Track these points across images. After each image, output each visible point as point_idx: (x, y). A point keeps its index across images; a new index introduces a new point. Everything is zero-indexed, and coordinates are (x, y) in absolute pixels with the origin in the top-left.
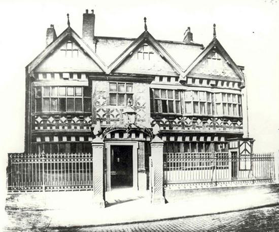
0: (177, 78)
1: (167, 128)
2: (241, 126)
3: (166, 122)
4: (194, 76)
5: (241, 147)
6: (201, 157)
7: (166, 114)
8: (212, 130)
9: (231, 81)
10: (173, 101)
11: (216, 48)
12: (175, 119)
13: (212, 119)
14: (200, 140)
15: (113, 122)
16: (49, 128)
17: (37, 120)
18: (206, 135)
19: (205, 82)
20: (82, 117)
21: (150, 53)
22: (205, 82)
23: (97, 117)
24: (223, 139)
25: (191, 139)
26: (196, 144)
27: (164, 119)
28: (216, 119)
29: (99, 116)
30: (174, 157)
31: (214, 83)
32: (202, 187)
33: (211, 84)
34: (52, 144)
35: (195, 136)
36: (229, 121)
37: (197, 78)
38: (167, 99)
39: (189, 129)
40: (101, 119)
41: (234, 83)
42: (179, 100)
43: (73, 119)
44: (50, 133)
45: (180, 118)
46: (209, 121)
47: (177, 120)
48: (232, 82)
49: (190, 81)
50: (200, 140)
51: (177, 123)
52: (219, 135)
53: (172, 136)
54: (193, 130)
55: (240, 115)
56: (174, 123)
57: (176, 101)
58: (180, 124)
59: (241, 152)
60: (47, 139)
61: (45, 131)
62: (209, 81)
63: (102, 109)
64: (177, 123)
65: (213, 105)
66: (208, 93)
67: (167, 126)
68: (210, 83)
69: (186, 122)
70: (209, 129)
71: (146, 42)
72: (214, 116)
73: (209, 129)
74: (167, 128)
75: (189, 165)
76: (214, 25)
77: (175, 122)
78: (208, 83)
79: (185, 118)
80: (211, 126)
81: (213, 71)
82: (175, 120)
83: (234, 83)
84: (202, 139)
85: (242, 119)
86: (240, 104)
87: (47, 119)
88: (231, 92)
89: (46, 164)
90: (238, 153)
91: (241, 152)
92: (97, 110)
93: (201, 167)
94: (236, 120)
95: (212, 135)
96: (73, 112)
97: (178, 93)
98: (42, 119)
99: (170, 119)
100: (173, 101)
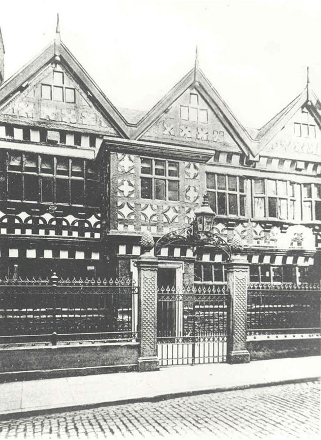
1: (74, 232)
10: (215, 189)
15: (145, 227)
16: (18, 232)
17: (97, 220)
19: (287, 164)
25: (261, 260)
37: (275, 158)
38: (227, 192)
39: (258, 243)
40: (127, 221)
41: (230, 156)
53: (207, 253)
54: (266, 245)
74: (74, 232)
76: (58, 15)
77: (89, 223)
82: (19, 215)
83: (230, 156)
84: (48, 254)
92: (119, 204)
98: (4, 215)
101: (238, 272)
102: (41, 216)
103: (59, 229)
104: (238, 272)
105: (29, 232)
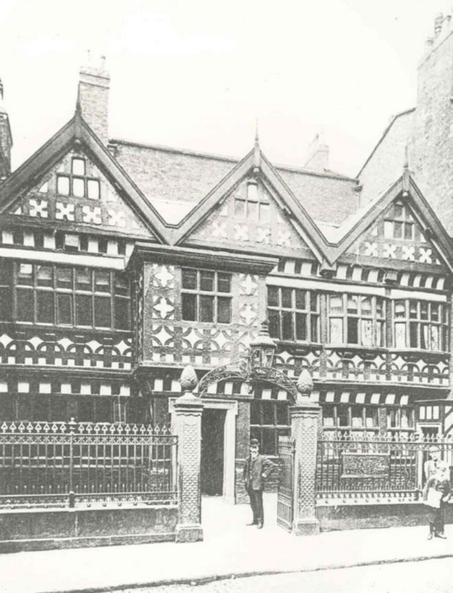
0: (315, 264)
1: (69, 361)
2: (446, 372)
3: (288, 361)
4: (352, 262)
5: (446, 420)
6: (343, 439)
7: (315, 343)
8: (383, 380)
9: (357, 266)
11: (405, 201)
12: (307, 354)
13: (384, 356)
14: (357, 401)
16: (29, 361)
18: (369, 390)
20: (109, 341)
21: (261, 203)
22: (373, 277)
23: (155, 344)
24: (404, 400)
26: (333, 407)
27: (421, 361)
28: (394, 356)
29: (158, 341)
30: (116, 432)
31: (394, 277)
32: (389, 501)
33: (386, 280)
34: (337, 406)
35: (347, 391)
36: (357, 357)
39: (334, 376)
42: (318, 312)
43: (60, 342)
44: (32, 372)
45: (318, 352)
46: (378, 361)
47: (311, 357)
48: (376, 269)
49: (341, 274)
50: (357, 401)
51: (311, 362)
52: (399, 391)
55: (444, 350)
56: (114, 353)
57: (312, 315)
58: (318, 364)
59: (446, 429)
60: (66, 389)
61: (388, 383)
62: (382, 272)
63: (166, 327)
64: (311, 362)
65: (388, 327)
66: (380, 299)
67: (291, 367)
68: (384, 278)
69: (330, 361)
70: (378, 378)
71: (77, 148)
72: (391, 349)
73: (378, 378)
75: (131, 454)
77: (117, 351)
78: (380, 278)
79: (394, 356)
80: (381, 372)
81: (71, 213)
85: (449, 357)
86: (447, 324)
87: (55, 340)
88: (342, 291)
89: (110, 446)
90: (440, 430)
91: (446, 429)
93: (116, 458)
94: (373, 355)
95: (384, 391)
96: (89, 327)
97: (316, 297)
98: (426, 364)
99: (79, 340)
100: (306, 315)
101: (306, 418)
102: (28, 341)
103: (108, 361)
104: (306, 418)
105: (42, 362)
